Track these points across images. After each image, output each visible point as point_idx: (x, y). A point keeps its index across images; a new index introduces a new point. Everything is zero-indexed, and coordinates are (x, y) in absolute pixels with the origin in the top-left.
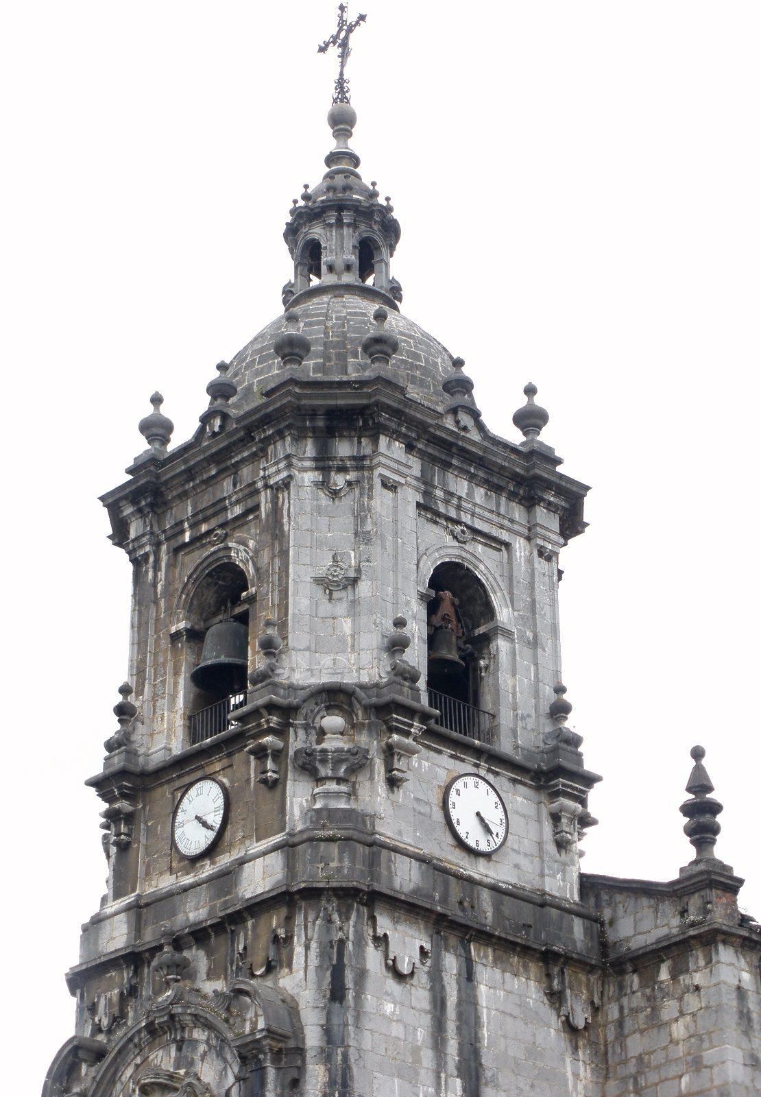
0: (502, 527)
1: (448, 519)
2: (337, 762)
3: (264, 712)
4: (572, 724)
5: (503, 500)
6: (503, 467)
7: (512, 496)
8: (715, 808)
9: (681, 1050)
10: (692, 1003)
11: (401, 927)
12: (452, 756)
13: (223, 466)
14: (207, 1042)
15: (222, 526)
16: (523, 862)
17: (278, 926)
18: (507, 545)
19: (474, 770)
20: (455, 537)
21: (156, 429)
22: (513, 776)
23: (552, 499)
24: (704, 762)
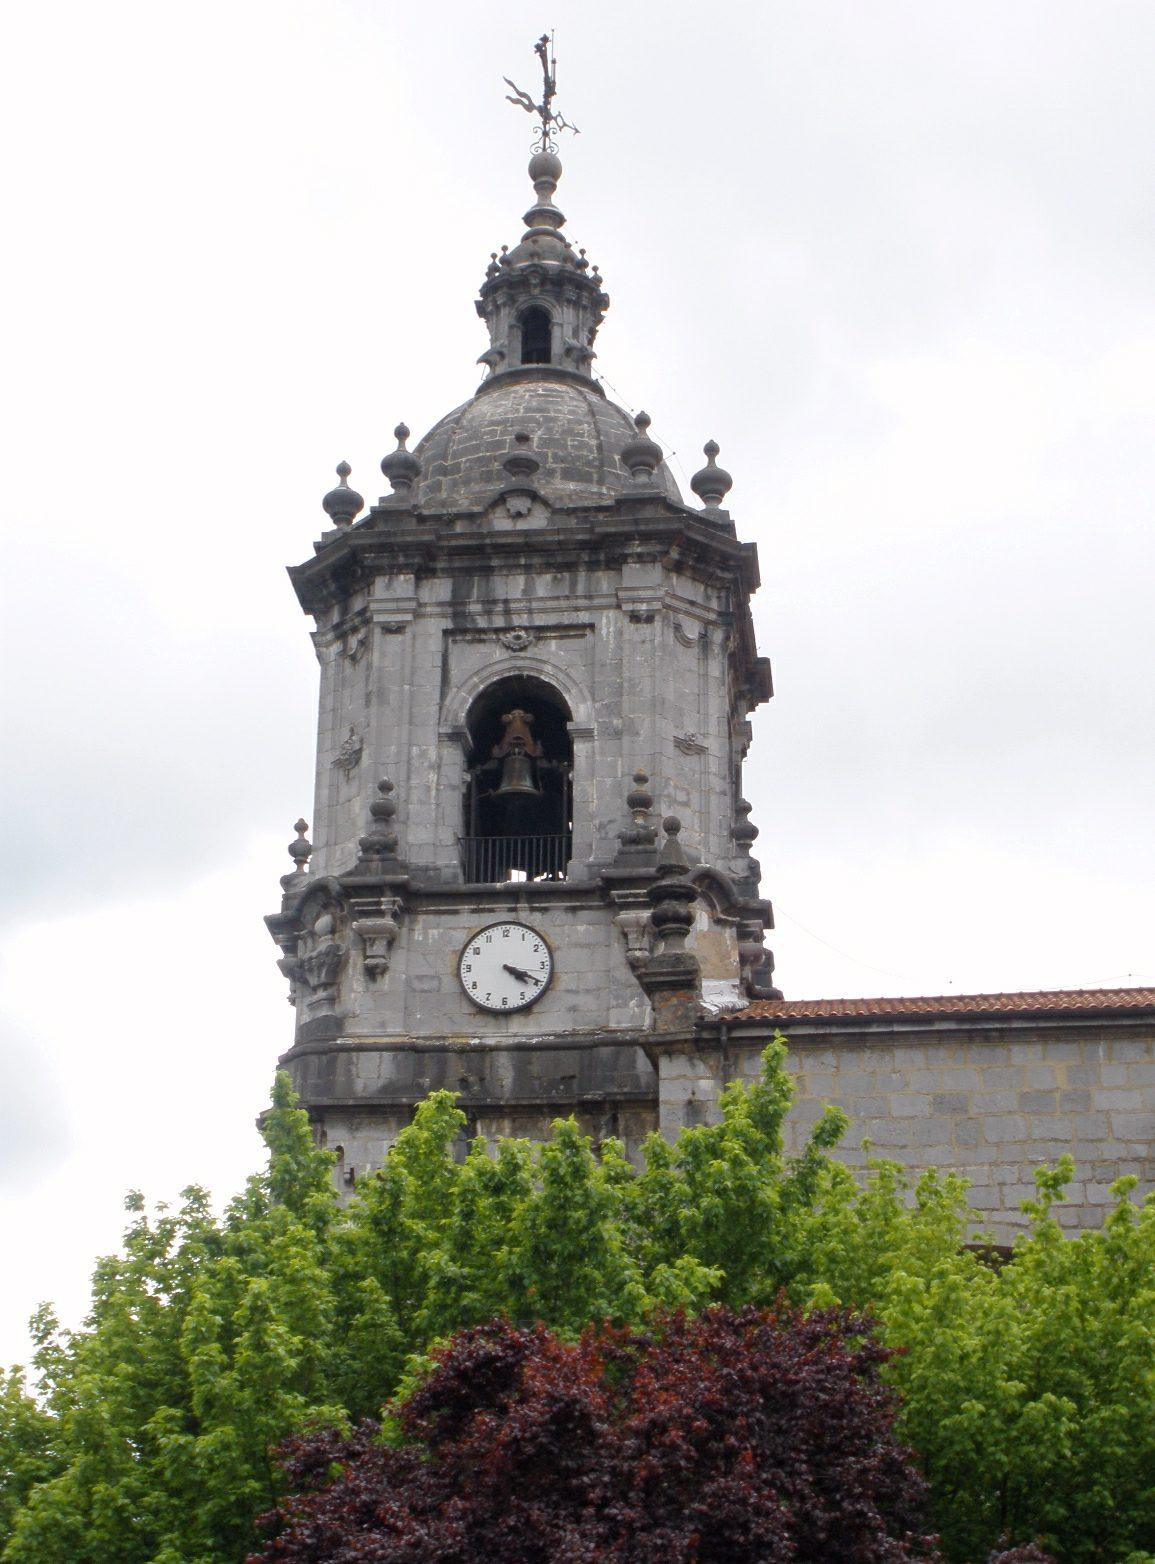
0: (577, 609)
1: (497, 631)
5: (582, 576)
6: (559, 542)
7: (593, 566)
11: (362, 1134)
12: (474, 911)
16: (580, 1000)
18: (592, 626)
19: (510, 917)
20: (508, 647)
21: (341, 504)
22: (568, 904)
23: (639, 550)
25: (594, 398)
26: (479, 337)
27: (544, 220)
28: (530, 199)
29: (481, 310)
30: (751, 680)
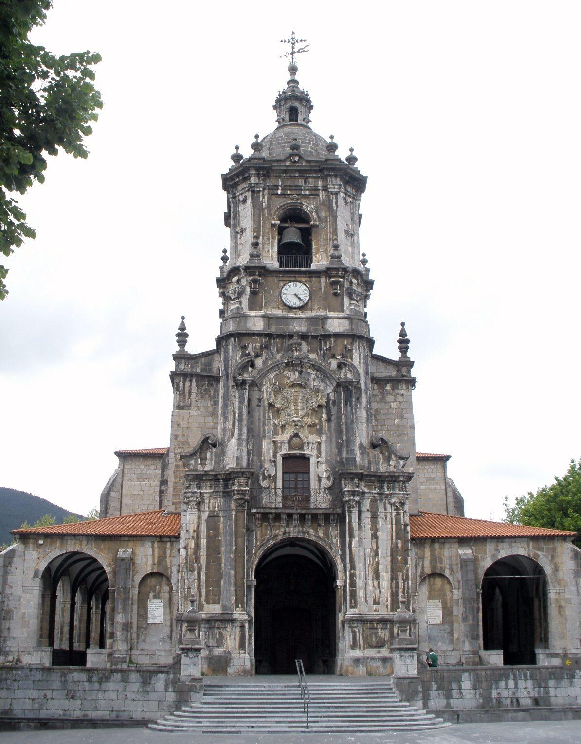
2: (358, 295)
3: (340, 270)
8: (408, 341)
9: (394, 411)
10: (400, 398)
13: (301, 174)
14: (316, 375)
15: (298, 195)
17: (348, 344)
21: (237, 158)
24: (405, 327)
27: (293, 82)
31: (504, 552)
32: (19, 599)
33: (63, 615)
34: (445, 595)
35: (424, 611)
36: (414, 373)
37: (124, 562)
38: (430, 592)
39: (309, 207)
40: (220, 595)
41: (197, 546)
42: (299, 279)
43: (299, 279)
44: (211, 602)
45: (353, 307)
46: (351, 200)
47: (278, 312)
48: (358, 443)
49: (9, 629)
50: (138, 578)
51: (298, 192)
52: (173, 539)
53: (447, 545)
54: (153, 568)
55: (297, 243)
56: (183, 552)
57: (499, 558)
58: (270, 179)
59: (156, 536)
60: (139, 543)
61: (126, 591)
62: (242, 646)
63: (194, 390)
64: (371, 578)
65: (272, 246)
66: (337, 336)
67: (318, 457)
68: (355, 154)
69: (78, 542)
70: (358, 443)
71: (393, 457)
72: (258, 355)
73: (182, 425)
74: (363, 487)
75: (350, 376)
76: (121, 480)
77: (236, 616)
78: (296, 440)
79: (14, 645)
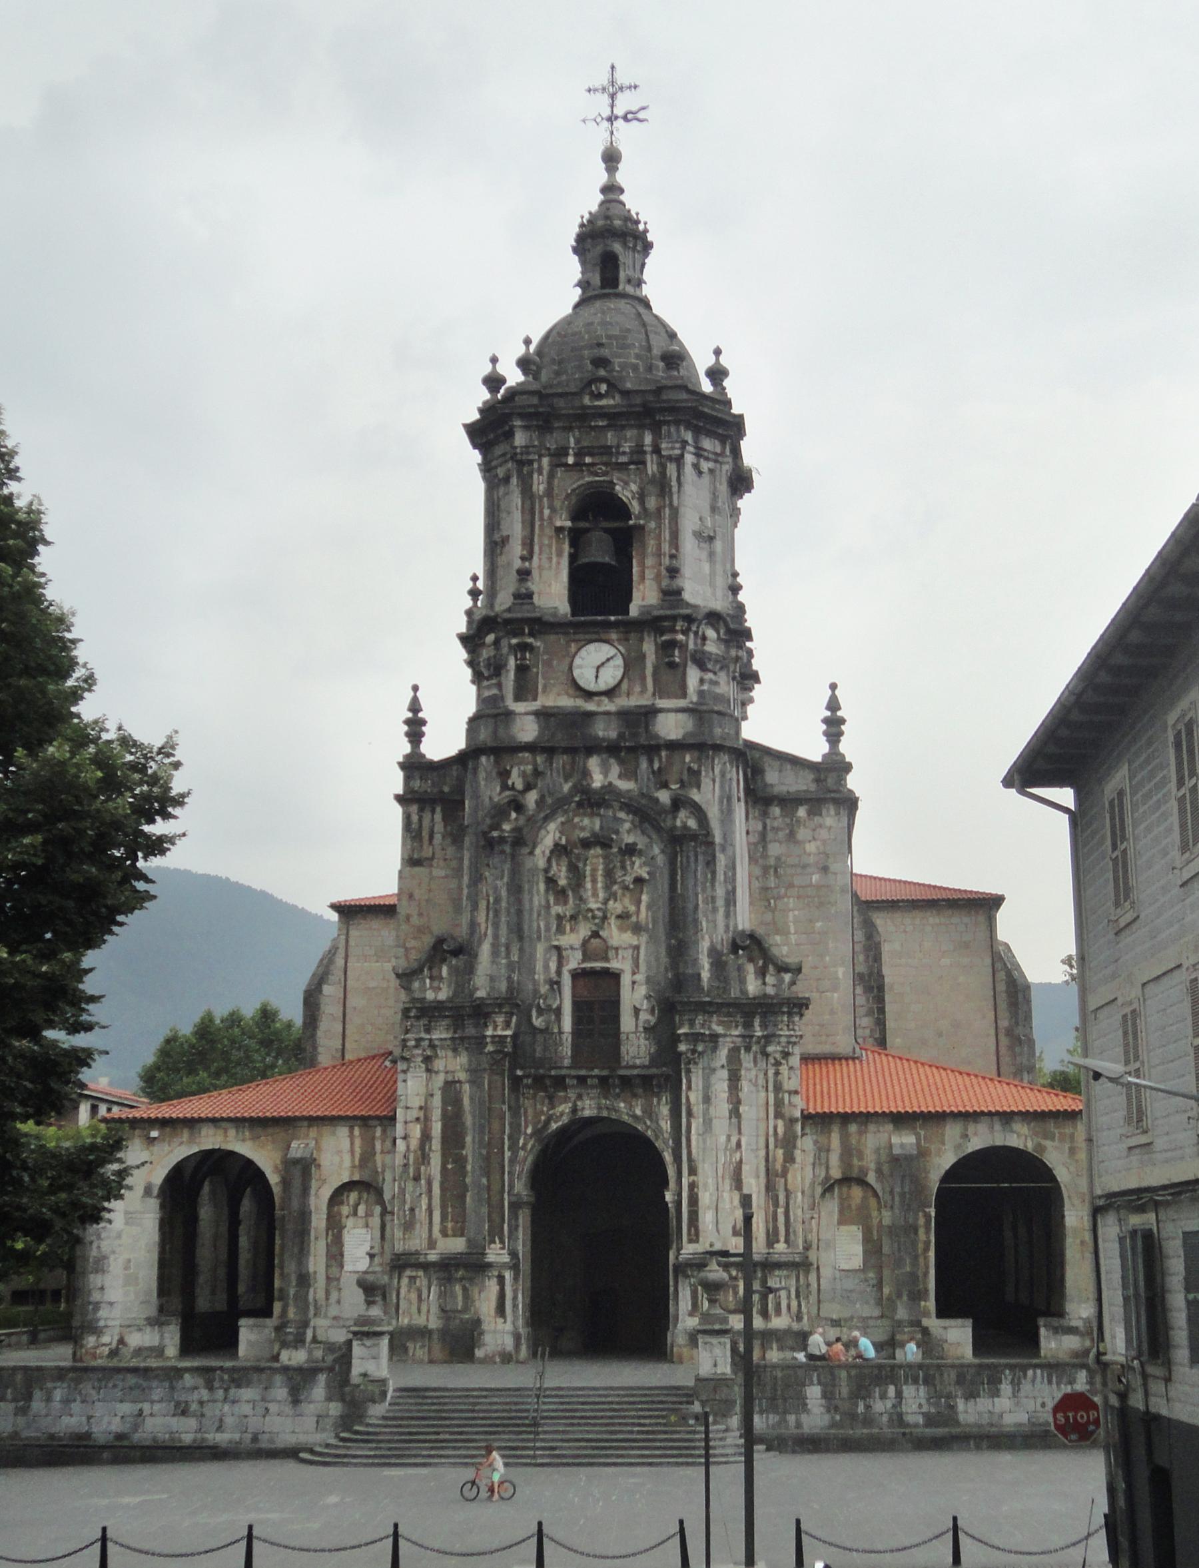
4: (741, 597)
8: (423, 722)
15: (605, 464)
21: (493, 382)
25: (642, 310)
26: (573, 268)
27: (611, 190)
28: (603, 178)
29: (576, 250)
30: (741, 482)
31: (980, 1139)
32: (119, 1236)
33: (215, 1247)
34: (869, 1216)
35: (830, 1245)
36: (853, 782)
37: (299, 1167)
38: (841, 1212)
39: (627, 491)
40: (464, 1222)
41: (426, 1137)
42: (603, 636)
43: (603, 636)
44: (450, 1232)
45: (705, 687)
46: (711, 465)
47: (566, 702)
48: (705, 945)
49: (102, 1288)
50: (326, 1193)
51: (605, 459)
52: (386, 1122)
53: (872, 1127)
54: (352, 1174)
55: (604, 564)
56: (401, 1145)
57: (970, 1150)
58: (552, 433)
59: (355, 1118)
60: (326, 1130)
61: (304, 1216)
62: (501, 1310)
63: (439, 827)
64: (727, 1187)
65: (557, 573)
66: (674, 746)
67: (634, 973)
68: (724, 360)
69: (220, 1132)
70: (705, 945)
71: (771, 968)
72: (528, 787)
73: (417, 894)
74: (714, 1027)
75: (692, 823)
76: (343, 962)
77: (491, 1258)
78: (595, 942)
79: (112, 1316)
